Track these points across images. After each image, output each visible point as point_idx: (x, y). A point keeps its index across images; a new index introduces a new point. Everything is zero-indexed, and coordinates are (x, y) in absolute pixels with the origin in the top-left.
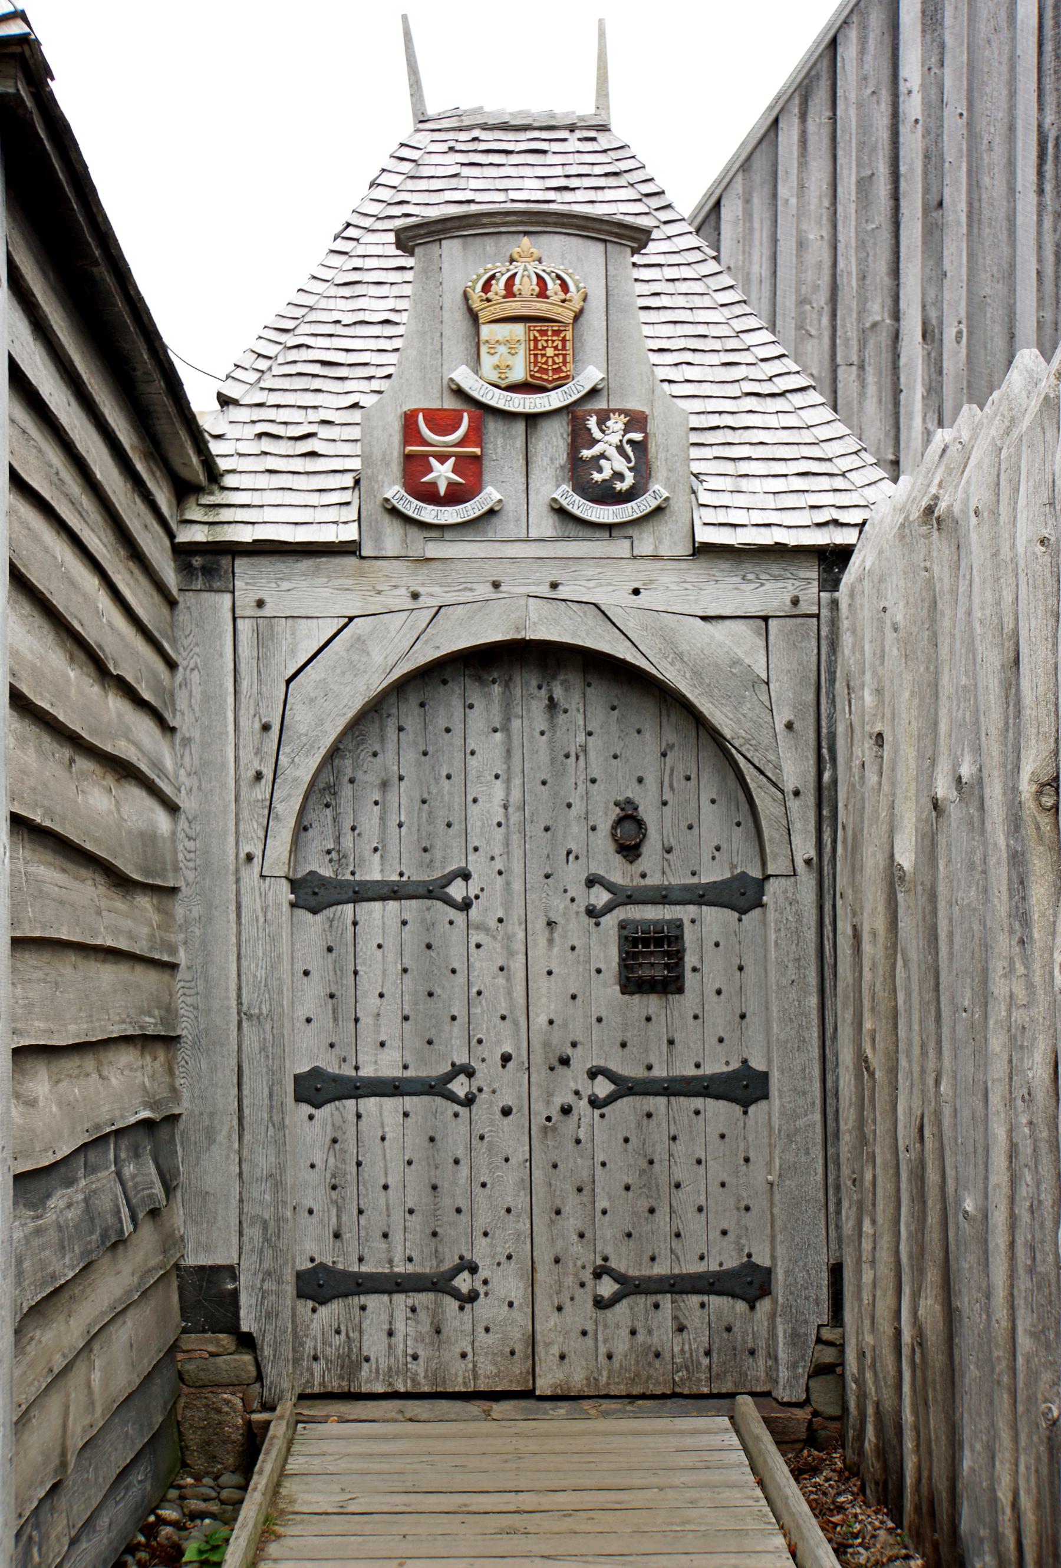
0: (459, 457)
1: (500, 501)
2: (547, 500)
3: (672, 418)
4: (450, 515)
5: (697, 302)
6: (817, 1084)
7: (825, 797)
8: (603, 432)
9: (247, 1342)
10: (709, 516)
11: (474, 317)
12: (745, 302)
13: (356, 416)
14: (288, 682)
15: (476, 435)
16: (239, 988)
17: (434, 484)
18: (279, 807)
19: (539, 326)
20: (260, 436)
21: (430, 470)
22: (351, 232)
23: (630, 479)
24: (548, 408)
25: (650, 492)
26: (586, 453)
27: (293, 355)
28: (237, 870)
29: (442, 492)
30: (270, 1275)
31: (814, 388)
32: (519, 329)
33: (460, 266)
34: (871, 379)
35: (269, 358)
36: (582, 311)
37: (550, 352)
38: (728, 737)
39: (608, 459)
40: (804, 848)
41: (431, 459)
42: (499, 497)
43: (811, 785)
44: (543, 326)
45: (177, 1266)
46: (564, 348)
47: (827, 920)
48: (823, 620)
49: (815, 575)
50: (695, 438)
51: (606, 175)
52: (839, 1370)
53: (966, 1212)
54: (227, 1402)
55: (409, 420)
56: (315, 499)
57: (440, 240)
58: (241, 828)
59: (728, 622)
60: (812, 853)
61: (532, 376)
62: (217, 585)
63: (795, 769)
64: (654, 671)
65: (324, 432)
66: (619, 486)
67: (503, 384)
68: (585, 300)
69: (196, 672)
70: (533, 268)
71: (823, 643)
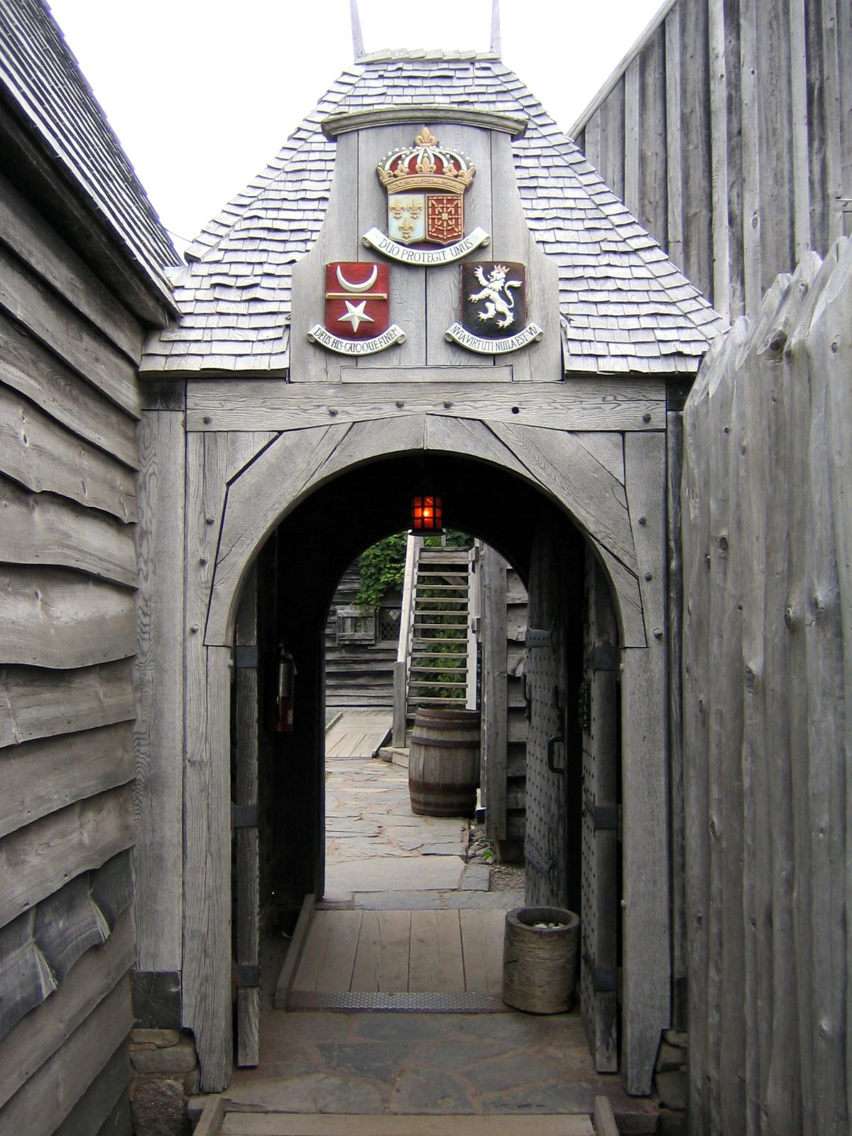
0: (369, 300)
1: (403, 336)
2: (442, 335)
3: (545, 274)
4: (362, 347)
5: (568, 183)
6: (664, 826)
7: (673, 582)
8: (488, 280)
9: (188, 1035)
10: (575, 348)
11: (384, 189)
12: (603, 183)
13: (287, 270)
14: (229, 484)
15: (384, 282)
16: (185, 739)
17: (349, 323)
18: (219, 588)
19: (436, 196)
20: (214, 286)
21: (346, 311)
22: (302, 135)
23: (510, 319)
24: (443, 261)
25: (527, 329)
26: (474, 297)
27: (248, 224)
28: (184, 640)
29: (355, 330)
30: (207, 981)
31: (659, 247)
32: (419, 199)
33: (373, 150)
34: (693, 253)
35: (228, 226)
36: (471, 184)
37: (445, 216)
38: (591, 531)
39: (491, 301)
40: (656, 624)
41: (347, 302)
42: (402, 333)
43: (661, 572)
44: (440, 196)
45: (131, 973)
46: (456, 212)
47: (674, 686)
48: (669, 434)
49: (663, 397)
50: (563, 286)
51: (497, 93)
52: (683, 1068)
53: (823, 1031)
54: (171, 1087)
55: (330, 271)
56: (252, 336)
57: (358, 131)
58: (188, 605)
59: (591, 435)
60: (661, 630)
61: (429, 235)
62: (172, 405)
63: (648, 557)
64: (529, 476)
65: (266, 282)
66: (501, 323)
67: (407, 241)
68: (473, 176)
69: (153, 477)
70: (433, 150)
71: (670, 453)
